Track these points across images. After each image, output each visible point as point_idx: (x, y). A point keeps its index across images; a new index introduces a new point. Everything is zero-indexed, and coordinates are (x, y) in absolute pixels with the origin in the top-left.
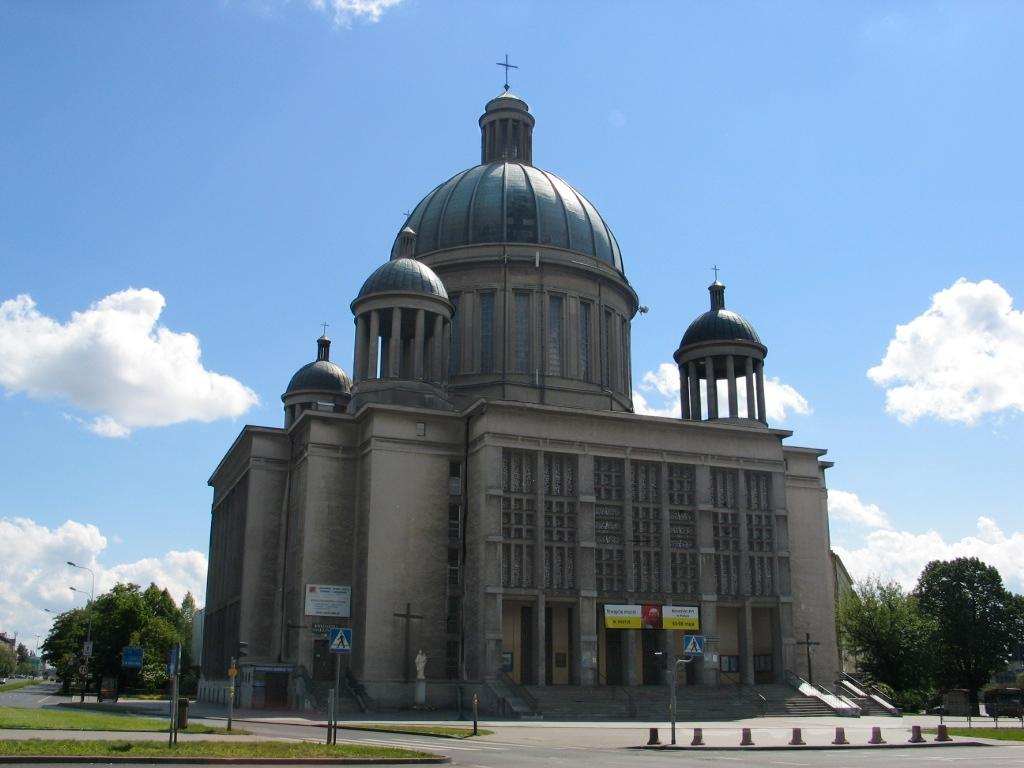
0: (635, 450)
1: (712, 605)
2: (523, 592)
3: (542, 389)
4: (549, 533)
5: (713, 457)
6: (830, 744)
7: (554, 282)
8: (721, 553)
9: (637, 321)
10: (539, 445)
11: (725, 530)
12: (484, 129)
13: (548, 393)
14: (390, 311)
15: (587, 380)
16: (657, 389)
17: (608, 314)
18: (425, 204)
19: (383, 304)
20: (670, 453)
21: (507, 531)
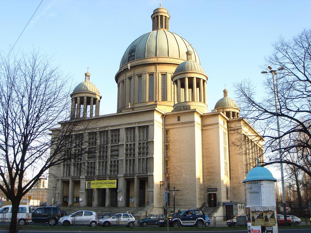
1: (121, 178)
2: (66, 178)
5: (126, 124)
7: (138, 71)
8: (128, 159)
10: (136, 125)
19: (182, 76)
21: (127, 155)
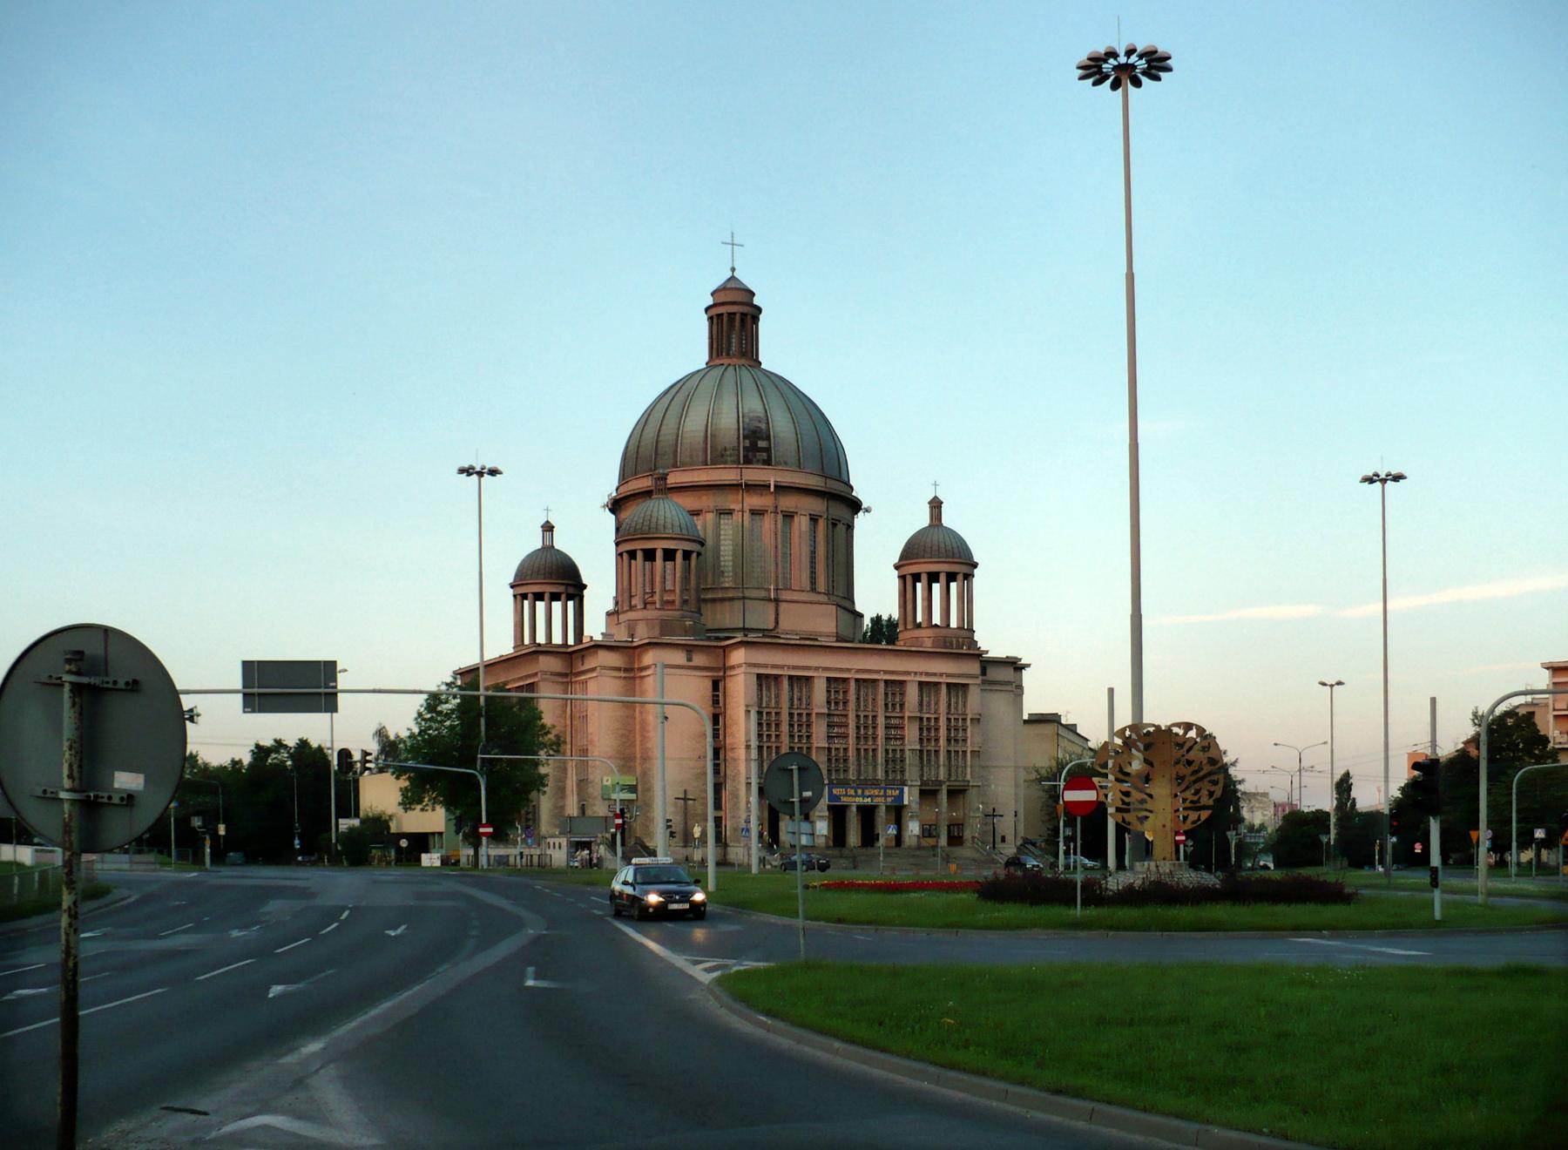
0: (858, 671)
3: (777, 601)
4: (792, 736)
6: (586, 633)
7: (788, 502)
9: (860, 520)
11: (927, 730)
12: (711, 319)
13: (783, 606)
14: (654, 550)
15: (813, 590)
16: (876, 592)
17: (834, 525)
18: (657, 415)
20: (886, 672)
